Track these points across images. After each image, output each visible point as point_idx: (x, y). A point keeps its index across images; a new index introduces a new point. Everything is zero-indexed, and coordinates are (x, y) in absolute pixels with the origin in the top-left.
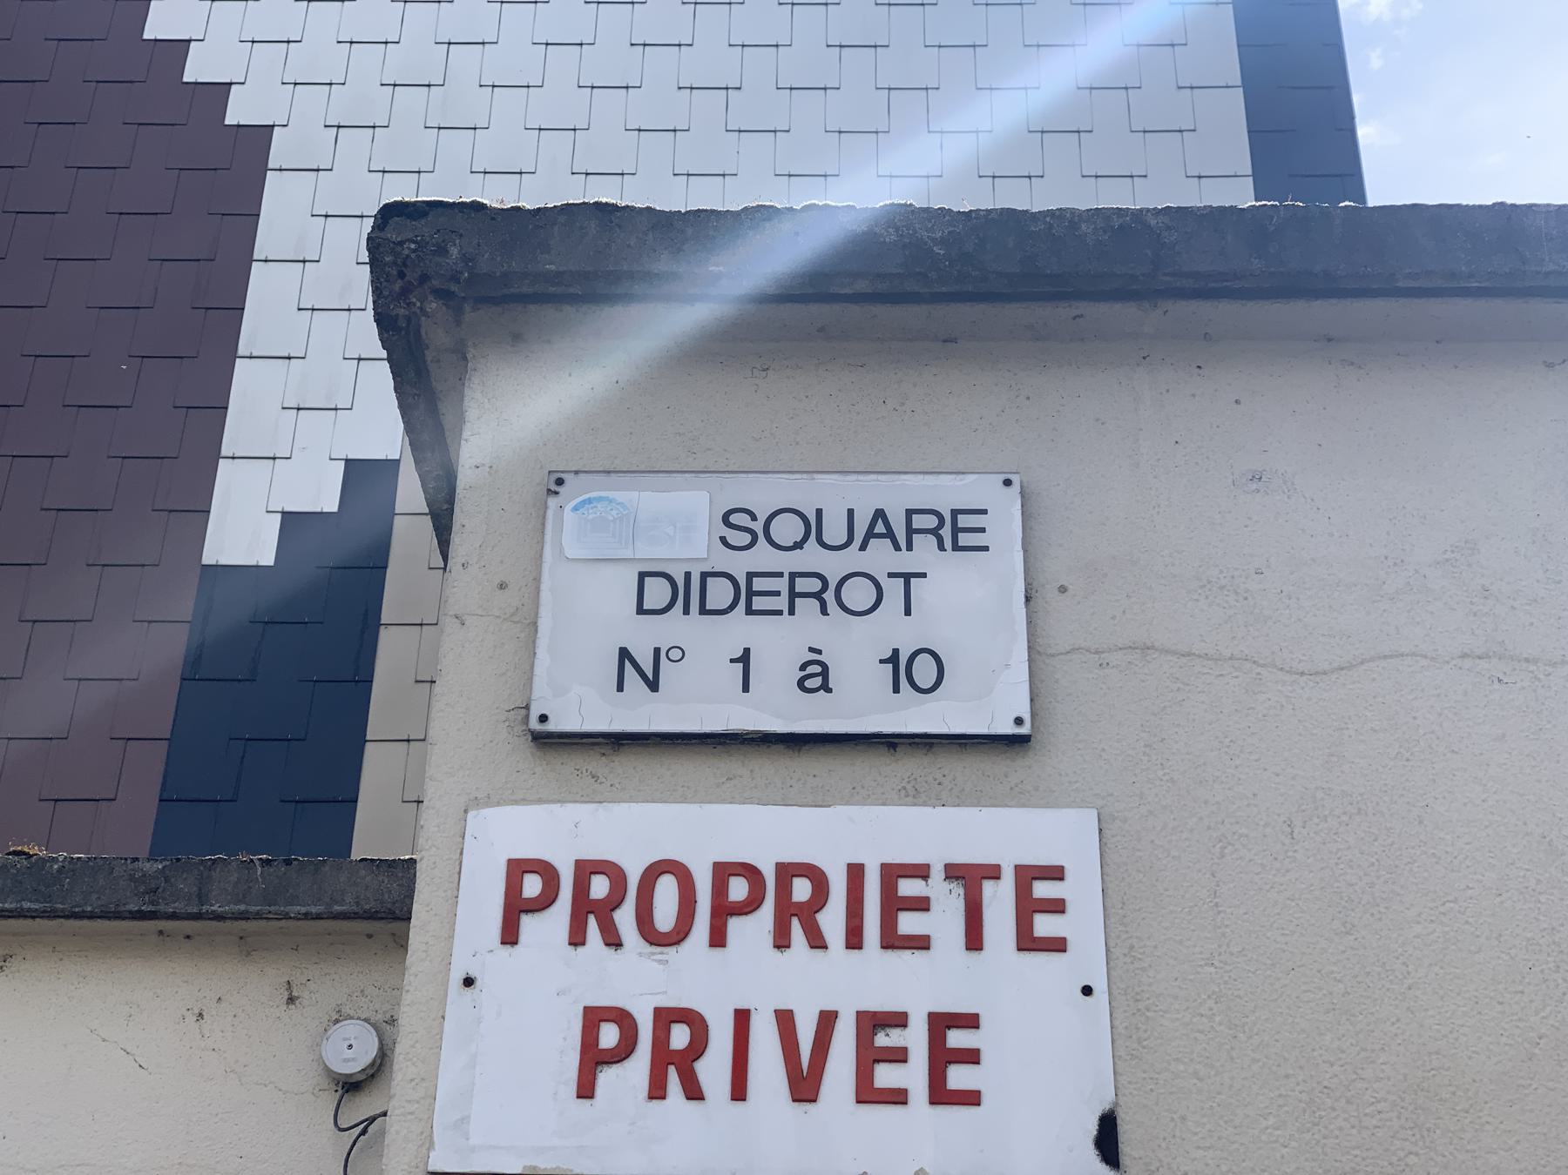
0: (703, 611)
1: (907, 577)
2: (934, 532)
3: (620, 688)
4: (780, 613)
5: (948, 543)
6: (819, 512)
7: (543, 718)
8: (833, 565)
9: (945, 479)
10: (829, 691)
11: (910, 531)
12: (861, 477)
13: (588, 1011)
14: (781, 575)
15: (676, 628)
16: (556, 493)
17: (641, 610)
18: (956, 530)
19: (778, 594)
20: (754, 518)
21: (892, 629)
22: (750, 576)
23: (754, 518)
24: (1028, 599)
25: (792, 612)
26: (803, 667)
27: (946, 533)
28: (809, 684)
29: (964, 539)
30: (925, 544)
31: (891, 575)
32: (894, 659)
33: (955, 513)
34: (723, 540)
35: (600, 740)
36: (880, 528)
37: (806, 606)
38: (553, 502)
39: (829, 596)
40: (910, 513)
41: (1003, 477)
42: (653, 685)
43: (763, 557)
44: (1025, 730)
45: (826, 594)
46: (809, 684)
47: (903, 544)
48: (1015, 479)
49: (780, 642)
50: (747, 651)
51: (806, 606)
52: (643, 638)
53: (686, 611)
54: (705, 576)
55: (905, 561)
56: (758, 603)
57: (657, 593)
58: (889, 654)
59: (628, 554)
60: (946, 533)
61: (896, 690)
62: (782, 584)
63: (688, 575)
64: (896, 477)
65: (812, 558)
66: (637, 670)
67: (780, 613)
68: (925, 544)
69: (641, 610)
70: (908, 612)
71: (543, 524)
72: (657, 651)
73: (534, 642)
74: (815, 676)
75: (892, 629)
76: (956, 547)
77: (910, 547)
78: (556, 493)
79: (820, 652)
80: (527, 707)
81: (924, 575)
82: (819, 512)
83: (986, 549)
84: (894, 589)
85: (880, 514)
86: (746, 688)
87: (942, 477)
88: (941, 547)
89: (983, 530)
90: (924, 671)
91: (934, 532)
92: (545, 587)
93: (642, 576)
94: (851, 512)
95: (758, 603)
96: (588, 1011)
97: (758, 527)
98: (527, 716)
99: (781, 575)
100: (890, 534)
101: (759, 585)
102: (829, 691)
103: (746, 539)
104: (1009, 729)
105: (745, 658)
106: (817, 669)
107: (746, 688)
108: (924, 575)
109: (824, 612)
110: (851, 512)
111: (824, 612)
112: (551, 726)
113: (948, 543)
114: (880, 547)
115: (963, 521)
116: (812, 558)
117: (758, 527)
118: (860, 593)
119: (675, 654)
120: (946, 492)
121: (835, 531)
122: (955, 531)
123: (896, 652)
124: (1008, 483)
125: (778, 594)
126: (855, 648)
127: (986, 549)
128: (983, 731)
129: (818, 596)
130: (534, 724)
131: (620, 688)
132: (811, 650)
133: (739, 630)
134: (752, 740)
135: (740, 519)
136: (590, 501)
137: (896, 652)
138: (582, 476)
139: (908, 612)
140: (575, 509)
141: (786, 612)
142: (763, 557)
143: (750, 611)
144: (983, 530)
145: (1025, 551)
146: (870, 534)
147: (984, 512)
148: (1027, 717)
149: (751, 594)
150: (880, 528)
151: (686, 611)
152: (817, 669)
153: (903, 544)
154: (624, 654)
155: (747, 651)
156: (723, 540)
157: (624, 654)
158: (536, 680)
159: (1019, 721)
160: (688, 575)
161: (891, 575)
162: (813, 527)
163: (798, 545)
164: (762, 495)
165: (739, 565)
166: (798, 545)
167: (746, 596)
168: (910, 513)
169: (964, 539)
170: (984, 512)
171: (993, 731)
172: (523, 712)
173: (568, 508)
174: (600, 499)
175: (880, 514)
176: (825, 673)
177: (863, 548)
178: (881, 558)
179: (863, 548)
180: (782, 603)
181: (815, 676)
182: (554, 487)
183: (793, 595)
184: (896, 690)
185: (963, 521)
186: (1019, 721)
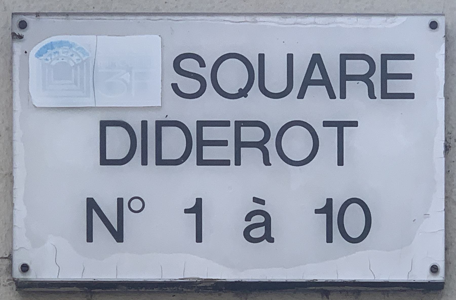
0: (160, 162)
1: (341, 126)
2: (366, 78)
3: (90, 239)
4: (226, 163)
5: (378, 92)
6: (261, 57)
7: (25, 268)
8: (274, 113)
9: (376, 22)
10: (271, 240)
11: (345, 78)
12: (299, 20)
13: (102, 164)
14: (226, 124)
15: (136, 179)
16: (21, 37)
17: (104, 161)
18: (385, 77)
19: (224, 143)
20: (202, 64)
21: (326, 180)
22: (201, 124)
23: (202, 64)
24: (447, 148)
25: (238, 163)
26: (248, 218)
27: (376, 79)
28: (254, 233)
29: (394, 86)
30: (356, 89)
31: (327, 124)
32: (327, 209)
33: (385, 58)
34: (175, 86)
35: (75, 289)
36: (317, 75)
37: (251, 156)
38: (18, 47)
39: (271, 145)
40: (344, 58)
41: (429, 19)
42: (118, 235)
43: (211, 106)
44: (439, 278)
45: (266, 143)
46: (254, 233)
47: (337, 93)
48: (441, 21)
49: (228, 191)
50: (199, 201)
51: (251, 156)
52: (109, 187)
53: (144, 162)
54: (160, 125)
55: (339, 110)
56: (209, 153)
57: (118, 142)
58: (322, 205)
59: (88, 102)
60: (376, 79)
61: (329, 239)
62: (227, 134)
63: (144, 124)
64: (332, 19)
65: (255, 106)
66: (105, 221)
67: (226, 163)
68: (356, 89)
69: (104, 161)
70: (340, 162)
71: (11, 71)
72: (120, 201)
73: (12, 193)
74: (259, 226)
75: (326, 180)
76: (385, 95)
77: (343, 96)
78: (21, 37)
79: (262, 202)
80: (10, 258)
81: (354, 124)
82: (261, 57)
83: (411, 96)
84: (328, 137)
85: (316, 59)
86: (199, 239)
87: (374, 18)
88: (372, 96)
89: (409, 76)
90: (354, 221)
91: (366, 78)
92: (18, 135)
93: (104, 125)
94: (290, 57)
95: (209, 153)
96: (102, 164)
97: (206, 73)
98: (11, 266)
99: (226, 124)
100: (325, 81)
101: (209, 133)
102: (271, 240)
103: (195, 86)
104: (424, 276)
105: (197, 209)
106: (259, 219)
107: (199, 239)
108: (354, 124)
109: (267, 162)
110: (290, 57)
111: (267, 162)
112: (32, 276)
113: (378, 92)
114: (317, 93)
115: (394, 67)
116: (255, 106)
117: (206, 73)
118: (297, 143)
119: (137, 205)
120: (376, 35)
121: (276, 80)
122: (383, 76)
123: (329, 201)
124: (434, 25)
125: (224, 143)
126: (294, 196)
127: (411, 96)
128: (403, 278)
129: (260, 145)
130: (18, 274)
131: (90, 239)
132: (256, 200)
133: (192, 181)
134: (205, 288)
135: (189, 65)
136: (51, 46)
137: (329, 201)
138: (44, 19)
139: (340, 162)
140: (39, 54)
141: (233, 162)
142: (211, 106)
143: (201, 162)
144: (409, 76)
145: (447, 98)
146: (308, 81)
147: (411, 57)
148: (441, 266)
149: (202, 143)
150: (317, 75)
151: (144, 162)
152: (259, 219)
153: (337, 93)
154: (92, 205)
155: (199, 201)
156: (175, 86)
157: (92, 205)
158: (16, 231)
159: (434, 269)
160: (144, 124)
161: (327, 124)
162: (256, 73)
163: (243, 93)
164: (210, 38)
165: (191, 113)
166: (243, 93)
167: (197, 145)
168: (344, 58)
169: (394, 86)
170: (411, 57)
171: (412, 279)
172: (7, 262)
173: (32, 54)
174: (61, 44)
175: (316, 59)
176: (267, 224)
177: (301, 96)
178: (317, 106)
179: (301, 96)
180: (228, 153)
181: (259, 226)
182: (18, 32)
183: (240, 145)
184: (329, 239)
185: (394, 67)
186: (434, 269)
